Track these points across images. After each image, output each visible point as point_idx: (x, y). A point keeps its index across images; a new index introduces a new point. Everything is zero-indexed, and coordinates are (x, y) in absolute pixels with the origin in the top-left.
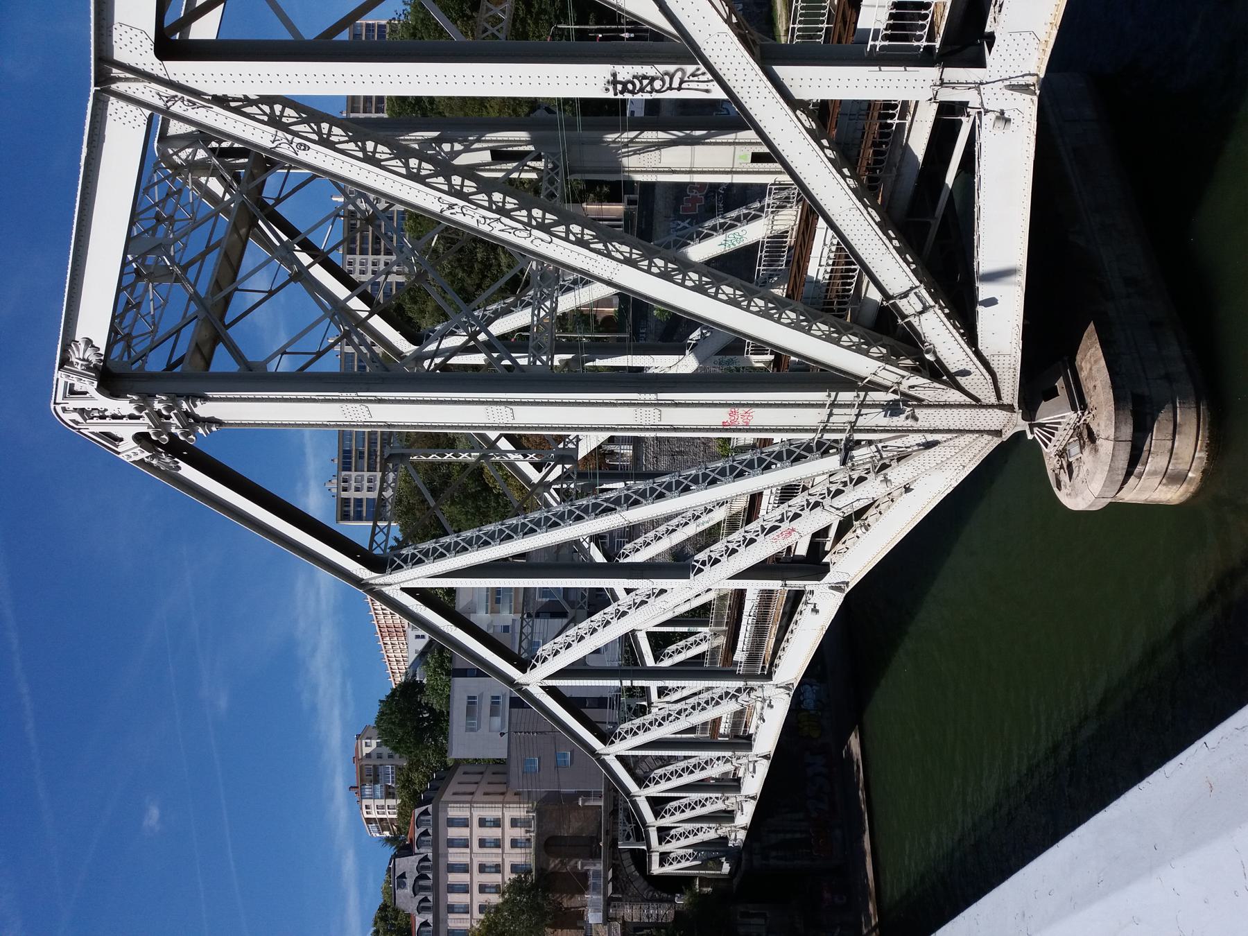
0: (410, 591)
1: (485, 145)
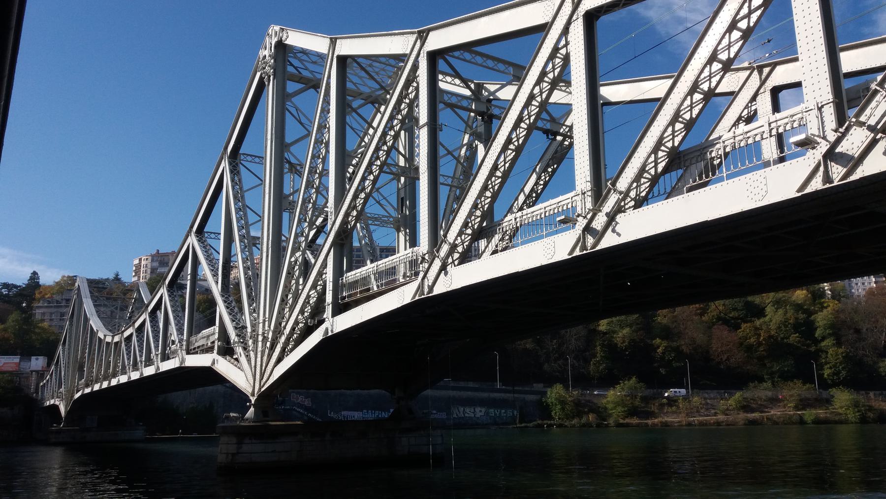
0: (838, 182)
1: (546, 89)
